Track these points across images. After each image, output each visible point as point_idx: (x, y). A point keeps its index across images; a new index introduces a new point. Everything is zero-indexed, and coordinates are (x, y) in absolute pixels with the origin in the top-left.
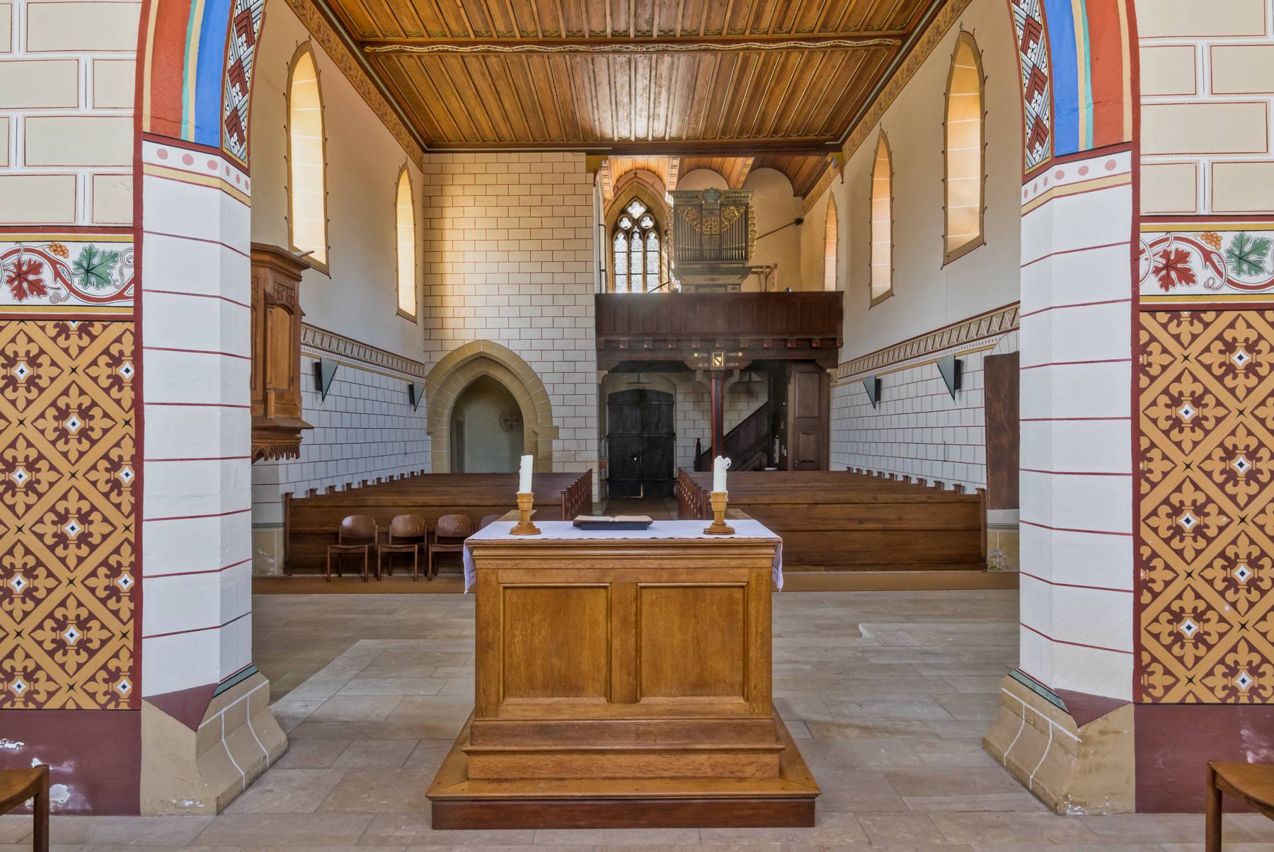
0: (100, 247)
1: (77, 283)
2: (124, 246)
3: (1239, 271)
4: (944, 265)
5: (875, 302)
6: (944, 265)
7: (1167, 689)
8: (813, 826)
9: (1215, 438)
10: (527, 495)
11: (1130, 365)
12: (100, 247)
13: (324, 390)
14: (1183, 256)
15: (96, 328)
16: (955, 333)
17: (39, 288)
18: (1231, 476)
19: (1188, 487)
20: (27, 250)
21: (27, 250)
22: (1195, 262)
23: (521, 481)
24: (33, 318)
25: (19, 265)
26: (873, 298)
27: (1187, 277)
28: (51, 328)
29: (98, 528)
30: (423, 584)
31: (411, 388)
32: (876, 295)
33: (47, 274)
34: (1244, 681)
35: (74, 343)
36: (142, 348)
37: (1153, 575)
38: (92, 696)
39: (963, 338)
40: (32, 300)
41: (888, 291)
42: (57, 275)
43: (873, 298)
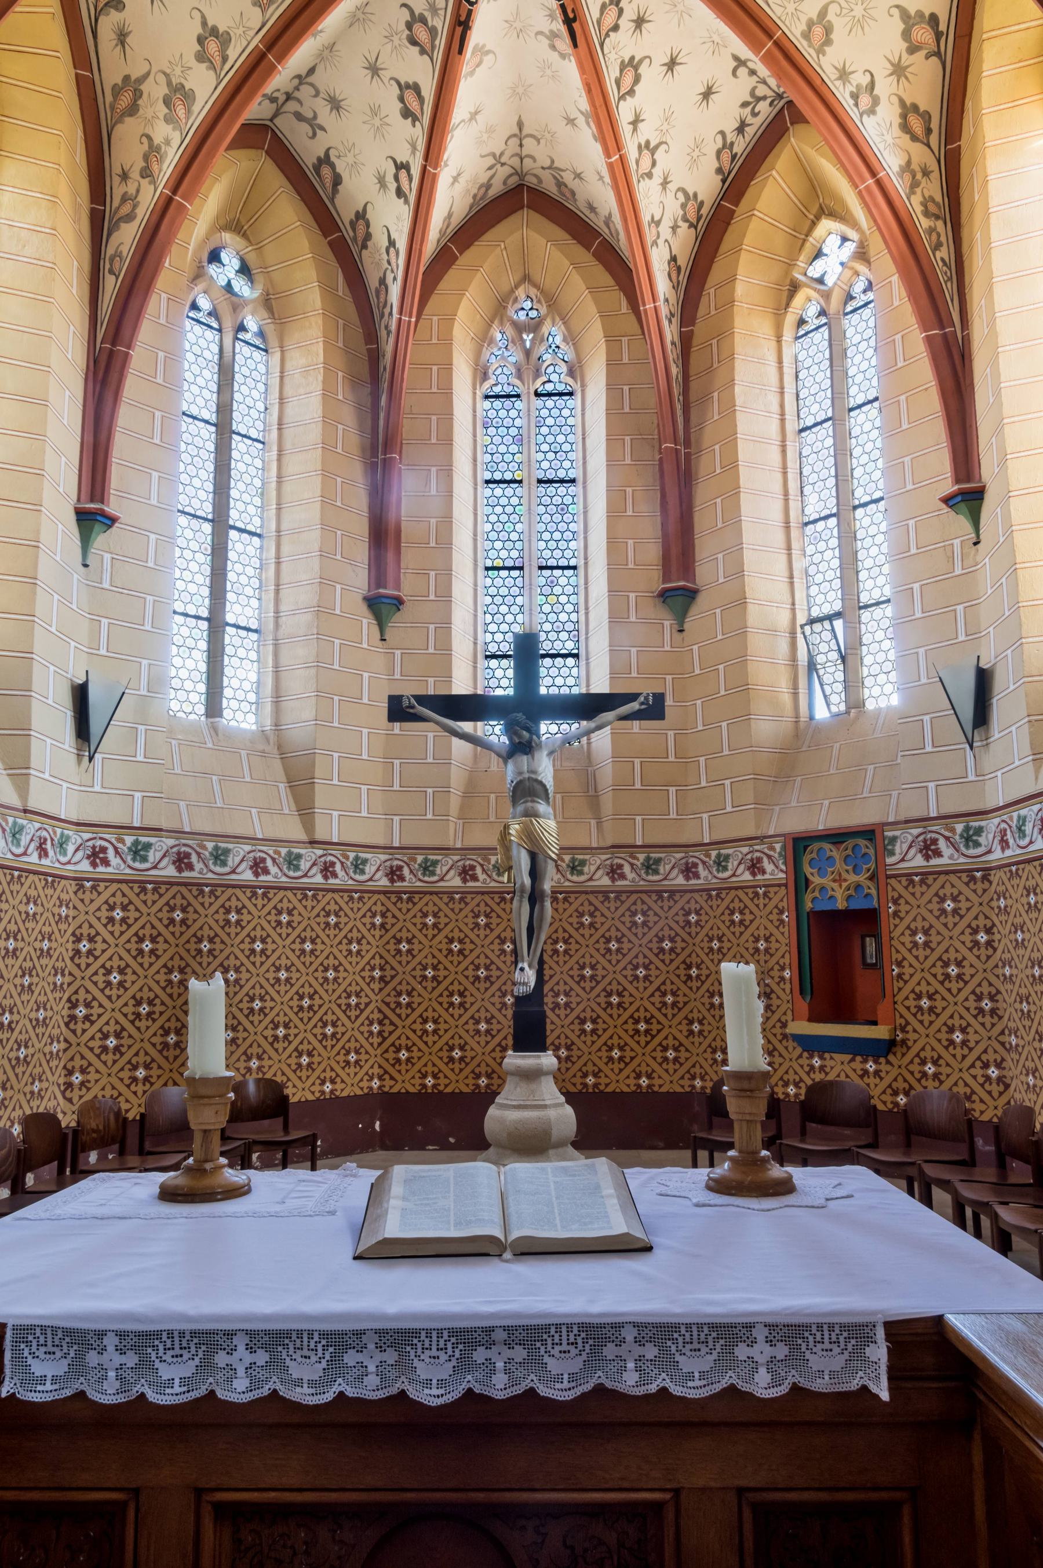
0: (141, 839)
1: (129, 858)
3: (647, 874)
7: (446, 1086)
9: (443, 1067)
12: (141, 839)
14: (620, 866)
15: (677, 897)
17: (475, 878)
18: (946, 965)
19: (466, 973)
20: (185, 845)
21: (185, 845)
22: (627, 869)
24: (741, 888)
25: (687, 863)
28: (601, 897)
29: (737, 904)
33: (111, 853)
34: (590, 1080)
35: (666, 904)
37: (974, 1106)
38: (885, 1103)
40: (331, 881)
42: (411, 872)
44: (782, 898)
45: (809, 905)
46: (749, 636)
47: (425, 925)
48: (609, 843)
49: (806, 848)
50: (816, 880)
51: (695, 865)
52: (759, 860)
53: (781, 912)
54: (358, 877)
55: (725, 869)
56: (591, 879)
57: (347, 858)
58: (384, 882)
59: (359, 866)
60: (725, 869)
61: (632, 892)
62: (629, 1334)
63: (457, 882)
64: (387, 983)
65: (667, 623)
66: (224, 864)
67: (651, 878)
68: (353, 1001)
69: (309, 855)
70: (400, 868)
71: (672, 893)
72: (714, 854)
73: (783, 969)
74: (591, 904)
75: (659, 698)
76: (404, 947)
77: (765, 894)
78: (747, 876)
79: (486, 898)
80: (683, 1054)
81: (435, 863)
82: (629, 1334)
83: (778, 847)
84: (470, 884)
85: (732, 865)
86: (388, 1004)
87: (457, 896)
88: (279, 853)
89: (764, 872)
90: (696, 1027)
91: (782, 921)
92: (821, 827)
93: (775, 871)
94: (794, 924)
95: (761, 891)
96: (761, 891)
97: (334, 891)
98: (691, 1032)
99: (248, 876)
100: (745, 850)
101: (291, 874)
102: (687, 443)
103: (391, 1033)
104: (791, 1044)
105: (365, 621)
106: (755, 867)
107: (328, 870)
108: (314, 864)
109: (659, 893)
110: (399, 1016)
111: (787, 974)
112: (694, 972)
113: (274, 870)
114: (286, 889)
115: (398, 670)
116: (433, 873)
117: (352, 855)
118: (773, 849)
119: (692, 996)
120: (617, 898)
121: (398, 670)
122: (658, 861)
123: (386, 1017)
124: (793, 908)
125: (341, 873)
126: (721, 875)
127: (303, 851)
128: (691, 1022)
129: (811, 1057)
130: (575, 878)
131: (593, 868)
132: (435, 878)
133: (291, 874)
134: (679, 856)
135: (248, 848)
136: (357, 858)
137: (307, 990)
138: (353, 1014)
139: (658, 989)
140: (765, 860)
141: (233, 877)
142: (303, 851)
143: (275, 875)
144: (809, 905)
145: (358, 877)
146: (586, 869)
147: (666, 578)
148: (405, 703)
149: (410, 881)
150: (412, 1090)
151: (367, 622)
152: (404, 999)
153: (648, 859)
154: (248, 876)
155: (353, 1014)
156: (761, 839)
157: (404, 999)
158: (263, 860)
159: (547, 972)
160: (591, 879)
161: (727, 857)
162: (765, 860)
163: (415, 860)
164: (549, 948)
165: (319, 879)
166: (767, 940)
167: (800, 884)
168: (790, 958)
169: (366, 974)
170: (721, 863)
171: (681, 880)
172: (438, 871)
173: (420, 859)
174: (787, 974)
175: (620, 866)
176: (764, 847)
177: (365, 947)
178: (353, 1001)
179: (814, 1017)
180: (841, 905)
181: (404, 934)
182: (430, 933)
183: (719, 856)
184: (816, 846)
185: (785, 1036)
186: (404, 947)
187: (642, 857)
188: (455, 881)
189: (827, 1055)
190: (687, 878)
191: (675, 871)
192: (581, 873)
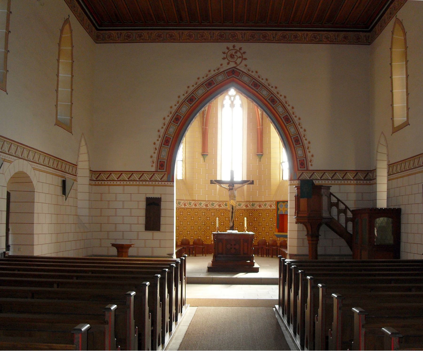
2: (305, 169)
4: (393, 133)
5: (396, 130)
6: (393, 133)
8: (161, 198)
10: (287, 181)
11: (377, 190)
13: (67, 194)
14: (248, 205)
16: (412, 162)
17: (197, 206)
22: (249, 205)
23: (218, 166)
26: (395, 126)
27: (261, 207)
30: (271, 259)
31: (64, 182)
32: (396, 124)
36: (7, 199)
39: (416, 164)
40: (196, 207)
41: (406, 122)
43: (395, 126)
44: (275, 212)
45: (279, 213)
46: (271, 170)
47: (212, 215)
48: (246, 201)
49: (279, 203)
50: (280, 209)
51: (261, 205)
52: (271, 205)
53: (274, 214)
54: (200, 206)
55: (266, 206)
56: (242, 207)
57: (198, 203)
58: (205, 207)
59: (200, 204)
60: (266, 206)
61: (249, 210)
62: (286, 209)
63: (218, 207)
64: (205, 225)
65: (258, 160)
66: (180, 205)
67: (253, 207)
68: (200, 228)
69: (193, 202)
70: (208, 204)
71: (257, 210)
72: (264, 203)
73: (274, 224)
74: (242, 212)
75: (253, 181)
76: (208, 219)
77: (272, 211)
78: (269, 208)
79: (223, 210)
80: (258, 238)
81: (214, 204)
82: (286, 209)
83: (274, 203)
84: (220, 207)
85: (267, 205)
86: (205, 229)
87: (218, 210)
88: (188, 202)
89: (272, 207)
90: (260, 234)
91: (274, 216)
92: (281, 200)
93: (274, 207)
94: (276, 226)
95: (271, 210)
96: (271, 210)
97: (196, 209)
98: (259, 234)
99: (183, 206)
100: (269, 203)
101: (190, 206)
102: (262, 125)
103: (206, 234)
104: (275, 236)
105: (201, 158)
106: (271, 206)
107: (195, 205)
108: (193, 204)
109: (254, 210)
110: (207, 231)
111: (275, 224)
112: (260, 224)
113: (187, 205)
114: (189, 208)
115: (207, 167)
116: (213, 205)
117: (199, 202)
118: (274, 203)
119: (260, 228)
120: (247, 211)
121: (207, 167)
122: (254, 204)
123: (205, 231)
124: (276, 223)
125: (198, 206)
126: (265, 207)
127: (191, 202)
128: (259, 233)
129: (278, 238)
130: (239, 207)
131: (243, 205)
132: (214, 206)
133: (190, 206)
134: (258, 203)
135: (183, 201)
136: (200, 203)
137: (192, 226)
138: (200, 230)
139: (254, 227)
140: (272, 205)
141: (181, 206)
142: (191, 202)
143: (187, 206)
144: (279, 213)
145: (200, 206)
146: (241, 205)
147: (258, 152)
148: (213, 182)
149: (209, 207)
150: (209, 244)
151: (202, 159)
152: (208, 228)
153: (253, 204)
154: (183, 206)
155: (200, 230)
156: (272, 201)
157: (208, 228)
158: (186, 204)
159: (234, 224)
160: (242, 207)
161: (266, 204)
162: (272, 205)
163: (210, 203)
164: (234, 219)
165: (194, 207)
166: (272, 219)
167: (278, 209)
168: (275, 222)
169: (202, 223)
170: (265, 205)
171: (258, 208)
172: (214, 205)
173: (211, 203)
174: (275, 224)
175: (248, 205)
176: (272, 203)
177: (201, 218)
178: (200, 228)
179: (279, 232)
180: (283, 213)
181: (208, 216)
182: (213, 216)
183: (265, 204)
184: (280, 203)
185: (274, 235)
186: (208, 219)
187: (251, 203)
188: (217, 207)
189: (280, 238)
190: (260, 207)
191: (257, 206)
192: (240, 206)
